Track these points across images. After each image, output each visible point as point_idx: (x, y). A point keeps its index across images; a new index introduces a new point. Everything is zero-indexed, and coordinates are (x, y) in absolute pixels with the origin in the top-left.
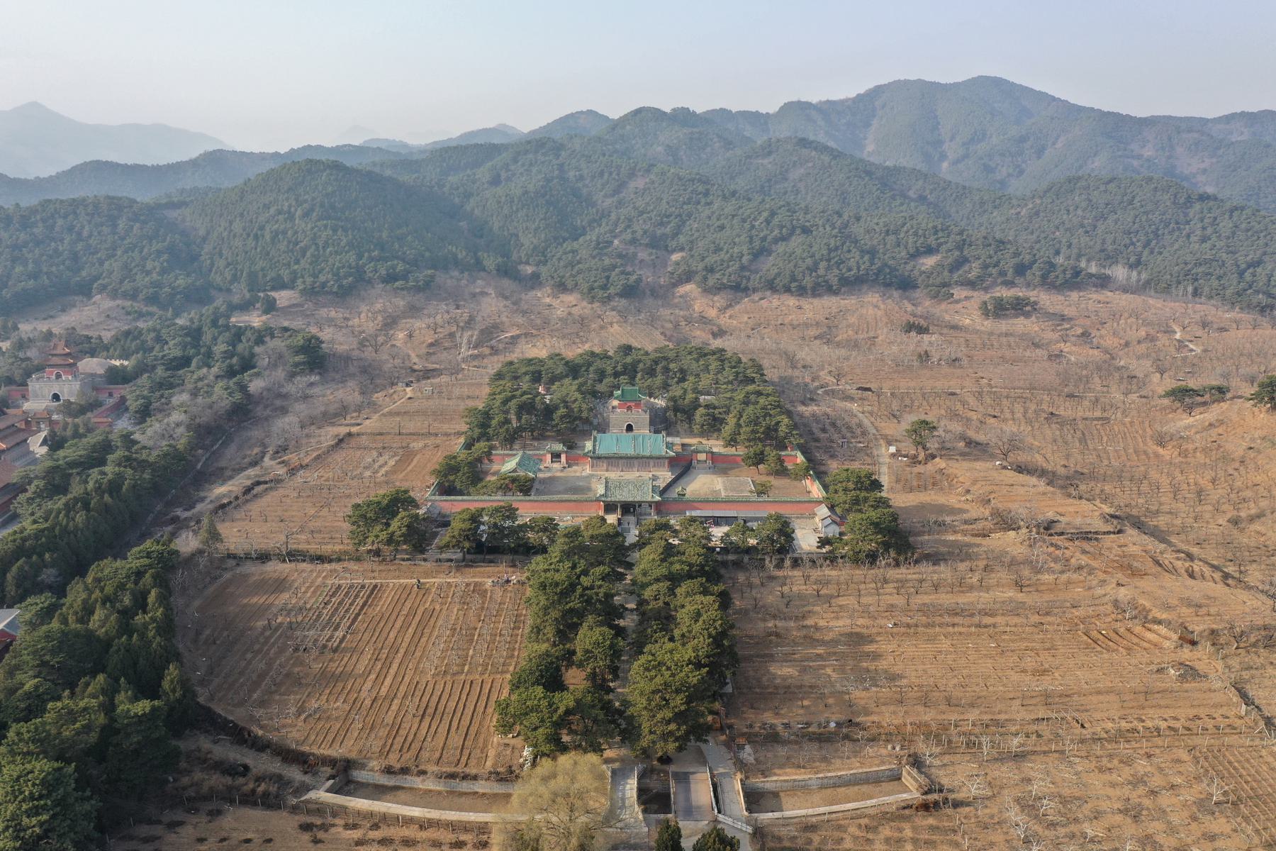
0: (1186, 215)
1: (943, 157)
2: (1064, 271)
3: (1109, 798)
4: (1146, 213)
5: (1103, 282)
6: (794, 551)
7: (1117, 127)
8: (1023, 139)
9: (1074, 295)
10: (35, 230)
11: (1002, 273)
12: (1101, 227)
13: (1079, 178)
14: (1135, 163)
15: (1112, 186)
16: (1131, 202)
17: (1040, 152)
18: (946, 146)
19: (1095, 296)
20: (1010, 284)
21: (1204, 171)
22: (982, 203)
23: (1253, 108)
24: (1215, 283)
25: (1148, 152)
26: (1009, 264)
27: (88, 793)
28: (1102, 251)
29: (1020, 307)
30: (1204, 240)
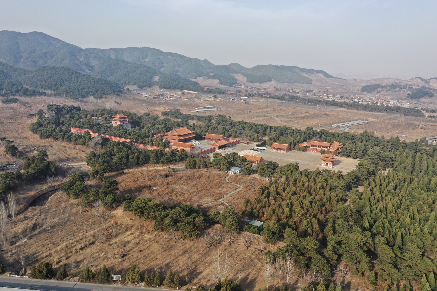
0: (71, 77)
1: (21, 57)
2: (30, 92)
3: (309, 181)
4: (61, 76)
5: (44, 94)
6: (278, 166)
7: (74, 51)
8: (46, 53)
9: (33, 98)
10: (124, 150)
11: (12, 92)
12: (49, 80)
13: (46, 67)
14: (77, 62)
15: (53, 70)
16: (58, 74)
17: (52, 58)
18: (22, 54)
19: (38, 97)
20: (14, 95)
21: (97, 65)
22: (21, 73)
23: (116, 47)
24: (72, 93)
25: (81, 59)
26: (14, 90)
27: (259, 265)
28: (48, 86)
29: (14, 101)
30: (73, 83)
